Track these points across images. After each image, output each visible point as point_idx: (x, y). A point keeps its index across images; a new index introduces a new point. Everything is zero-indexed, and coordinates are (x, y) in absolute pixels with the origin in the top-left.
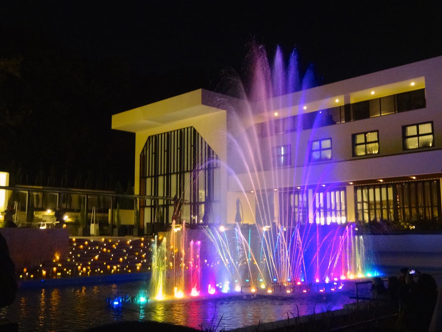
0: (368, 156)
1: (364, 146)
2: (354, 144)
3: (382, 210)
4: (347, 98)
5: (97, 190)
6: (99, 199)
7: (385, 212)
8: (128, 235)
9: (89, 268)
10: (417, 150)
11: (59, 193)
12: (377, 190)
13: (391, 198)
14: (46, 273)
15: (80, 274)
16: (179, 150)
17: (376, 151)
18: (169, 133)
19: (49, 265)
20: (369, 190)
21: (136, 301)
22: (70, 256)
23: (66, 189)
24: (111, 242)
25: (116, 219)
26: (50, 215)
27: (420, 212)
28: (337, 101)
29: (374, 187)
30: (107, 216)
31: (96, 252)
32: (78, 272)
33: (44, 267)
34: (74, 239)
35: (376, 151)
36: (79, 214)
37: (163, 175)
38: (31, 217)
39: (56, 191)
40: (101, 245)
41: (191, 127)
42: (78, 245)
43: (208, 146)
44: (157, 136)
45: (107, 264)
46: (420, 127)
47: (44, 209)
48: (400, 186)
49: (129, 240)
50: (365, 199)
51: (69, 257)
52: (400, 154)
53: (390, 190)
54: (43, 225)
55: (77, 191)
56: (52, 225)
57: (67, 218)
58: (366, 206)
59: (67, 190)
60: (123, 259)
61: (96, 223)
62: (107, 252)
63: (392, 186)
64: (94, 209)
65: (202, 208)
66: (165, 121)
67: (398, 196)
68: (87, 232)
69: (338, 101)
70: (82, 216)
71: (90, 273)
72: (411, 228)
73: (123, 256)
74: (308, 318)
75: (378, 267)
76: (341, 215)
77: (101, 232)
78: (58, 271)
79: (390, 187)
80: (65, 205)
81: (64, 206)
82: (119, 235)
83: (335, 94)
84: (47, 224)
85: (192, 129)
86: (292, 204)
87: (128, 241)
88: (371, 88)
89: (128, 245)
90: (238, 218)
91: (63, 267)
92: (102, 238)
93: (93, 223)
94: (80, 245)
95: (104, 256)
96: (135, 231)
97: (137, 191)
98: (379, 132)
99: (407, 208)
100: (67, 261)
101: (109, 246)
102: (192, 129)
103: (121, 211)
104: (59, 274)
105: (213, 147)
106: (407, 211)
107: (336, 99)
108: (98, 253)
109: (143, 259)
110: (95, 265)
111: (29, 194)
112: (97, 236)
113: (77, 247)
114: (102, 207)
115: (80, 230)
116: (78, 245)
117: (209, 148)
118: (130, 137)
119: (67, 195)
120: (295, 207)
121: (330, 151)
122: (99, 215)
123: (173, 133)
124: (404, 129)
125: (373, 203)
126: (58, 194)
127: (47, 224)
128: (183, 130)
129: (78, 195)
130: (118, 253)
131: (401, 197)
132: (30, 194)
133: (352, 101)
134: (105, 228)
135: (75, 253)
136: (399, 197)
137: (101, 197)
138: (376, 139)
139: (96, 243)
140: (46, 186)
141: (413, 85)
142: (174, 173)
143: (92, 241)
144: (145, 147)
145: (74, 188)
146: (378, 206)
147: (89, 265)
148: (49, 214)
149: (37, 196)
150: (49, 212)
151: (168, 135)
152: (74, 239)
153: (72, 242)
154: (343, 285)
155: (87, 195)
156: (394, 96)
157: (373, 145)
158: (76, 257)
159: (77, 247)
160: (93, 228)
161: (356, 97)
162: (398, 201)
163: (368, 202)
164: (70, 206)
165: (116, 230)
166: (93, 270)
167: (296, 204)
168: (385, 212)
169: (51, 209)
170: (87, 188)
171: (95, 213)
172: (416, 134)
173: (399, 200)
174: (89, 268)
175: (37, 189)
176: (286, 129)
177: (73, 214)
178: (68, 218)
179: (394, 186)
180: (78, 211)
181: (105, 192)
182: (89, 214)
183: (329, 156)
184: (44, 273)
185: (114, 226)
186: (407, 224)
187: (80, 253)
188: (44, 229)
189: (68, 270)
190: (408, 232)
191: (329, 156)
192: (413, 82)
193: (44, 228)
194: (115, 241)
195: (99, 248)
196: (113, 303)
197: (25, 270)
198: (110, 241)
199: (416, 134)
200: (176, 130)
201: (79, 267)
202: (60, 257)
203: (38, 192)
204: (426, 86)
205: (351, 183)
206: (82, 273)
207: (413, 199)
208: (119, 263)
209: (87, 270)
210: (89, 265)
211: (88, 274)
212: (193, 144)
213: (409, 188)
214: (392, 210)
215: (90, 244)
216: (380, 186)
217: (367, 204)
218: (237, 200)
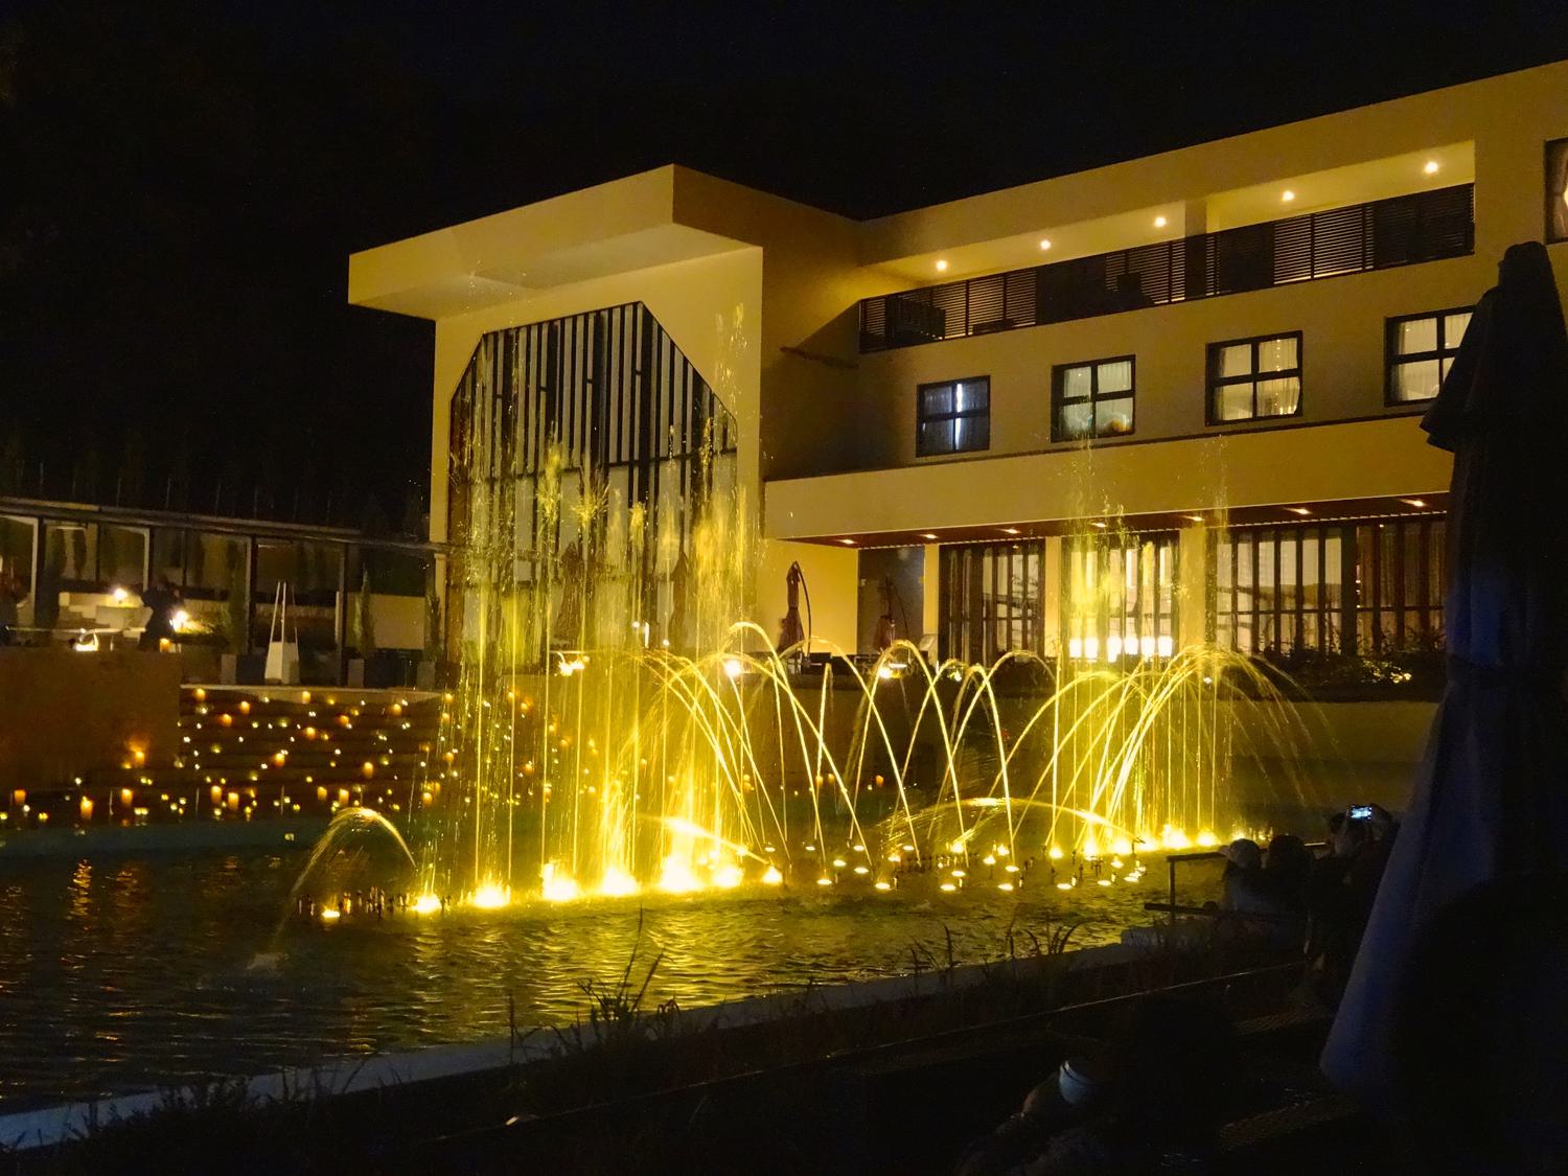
0: (1263, 422)
1: (1248, 387)
2: (1215, 381)
3: (1299, 612)
4: (1196, 215)
5: (297, 522)
6: (302, 552)
7: (1311, 621)
8: (402, 685)
9: (252, 794)
10: (1252, 426)
11: (152, 529)
12: (1288, 548)
13: (1334, 577)
14: (95, 808)
15: (218, 812)
16: (589, 387)
17: (1290, 408)
18: (603, 313)
19: (106, 776)
20: (1327, 541)
21: (405, 906)
22: (185, 751)
23: (184, 516)
24: (336, 704)
25: (357, 628)
26: (123, 605)
27: (1432, 624)
28: (1160, 222)
29: (1278, 537)
30: (331, 618)
31: (280, 740)
32: (208, 803)
33: (88, 789)
34: (201, 693)
35: (1290, 408)
36: (223, 607)
37: (625, 463)
38: (48, 611)
39: (141, 521)
40: (297, 714)
41: (635, 305)
42: (216, 713)
43: (695, 371)
44: (513, 333)
45: (317, 782)
46: (1103, 370)
47: (102, 587)
48: (1369, 534)
49: (398, 700)
50: (1245, 580)
51: (181, 754)
52: (1046, 452)
53: (1334, 546)
54: (88, 639)
55: (216, 524)
56: (119, 638)
57: (182, 621)
58: (1244, 602)
59: (188, 520)
60: (377, 766)
61: (290, 639)
62: (318, 740)
63: (1339, 530)
64: (281, 588)
65: (667, 593)
66: (537, 282)
67: (1358, 568)
68: (252, 670)
69: (1162, 224)
70: (236, 612)
71: (255, 811)
72: (1397, 679)
73: (374, 754)
74: (984, 971)
75: (1254, 813)
76: (1157, 633)
77: (307, 672)
78: (137, 801)
79: (1333, 536)
80: (181, 571)
81: (176, 576)
82: (366, 685)
83: (1153, 199)
84: (99, 635)
85: (640, 312)
86: (987, 588)
87: (395, 702)
88: (1285, 180)
89: (398, 717)
90: (792, 630)
91: (159, 786)
92: (302, 691)
93: (277, 639)
94: (222, 713)
95: (304, 753)
96: (428, 669)
97: (437, 531)
98: (1304, 336)
99: (1387, 609)
100: (174, 768)
101: (327, 718)
102: (640, 312)
103: (376, 598)
104: (141, 812)
105: (713, 383)
106: (1388, 622)
107: (938, 259)
108: (286, 745)
109: (444, 765)
110: (272, 783)
111: (42, 530)
112: (290, 684)
113: (211, 722)
114: (312, 586)
115: (228, 661)
116: (216, 713)
117: (699, 381)
118: (416, 336)
119: (187, 535)
120: (1011, 603)
121: (1127, 402)
122: (301, 611)
123: (523, 335)
124: (1393, 327)
125: (1272, 592)
126: (146, 533)
127: (99, 635)
128: (605, 314)
129: (227, 538)
130: (358, 744)
131: (1370, 570)
132: (45, 526)
133: (1214, 226)
134: (323, 658)
135: (202, 741)
136: (1364, 569)
137: (309, 548)
138: (1294, 365)
139: (279, 708)
140: (112, 503)
141: (1432, 170)
142: (619, 463)
143: (267, 700)
144: (470, 374)
145: (211, 513)
146: (1289, 604)
147: (250, 784)
148: (120, 602)
149: (78, 535)
150: (120, 597)
151: (553, 330)
152: (201, 693)
153: (195, 702)
154: (1143, 869)
155: (254, 537)
156: (1171, 247)
157: (1280, 383)
158: (207, 755)
159: (211, 722)
160: (278, 658)
161: (1230, 210)
162: (1357, 586)
163: (1255, 592)
164: (199, 576)
165: (357, 665)
166: (265, 799)
167: (1003, 591)
168: (1311, 621)
169: (124, 585)
170: (260, 517)
171: (284, 603)
172: (1433, 347)
173: (1363, 581)
174: (252, 794)
175: (74, 510)
176: (973, 322)
177: (209, 605)
178: (189, 621)
179: (1347, 532)
180: (224, 596)
181: (324, 529)
182: (261, 608)
183: (1125, 421)
184: (86, 804)
185: (350, 653)
186: (1386, 665)
187: (221, 742)
188: (94, 653)
189: (174, 799)
190: (1388, 691)
191: (1125, 421)
192: (1434, 158)
193: (93, 647)
194: (350, 704)
195: (292, 727)
196: (319, 911)
197: (20, 794)
198: (332, 702)
199: (1433, 347)
200: (568, 317)
201: (216, 790)
202: (149, 752)
203: (79, 522)
204: (1477, 176)
205: (931, 536)
206: (225, 811)
207: (1411, 580)
208: (362, 779)
209: (245, 801)
210: (250, 784)
211: (244, 816)
212: (642, 365)
213: (1400, 538)
214: (1335, 619)
215: (258, 709)
216: (1300, 532)
217: (1251, 597)
218: (793, 568)
